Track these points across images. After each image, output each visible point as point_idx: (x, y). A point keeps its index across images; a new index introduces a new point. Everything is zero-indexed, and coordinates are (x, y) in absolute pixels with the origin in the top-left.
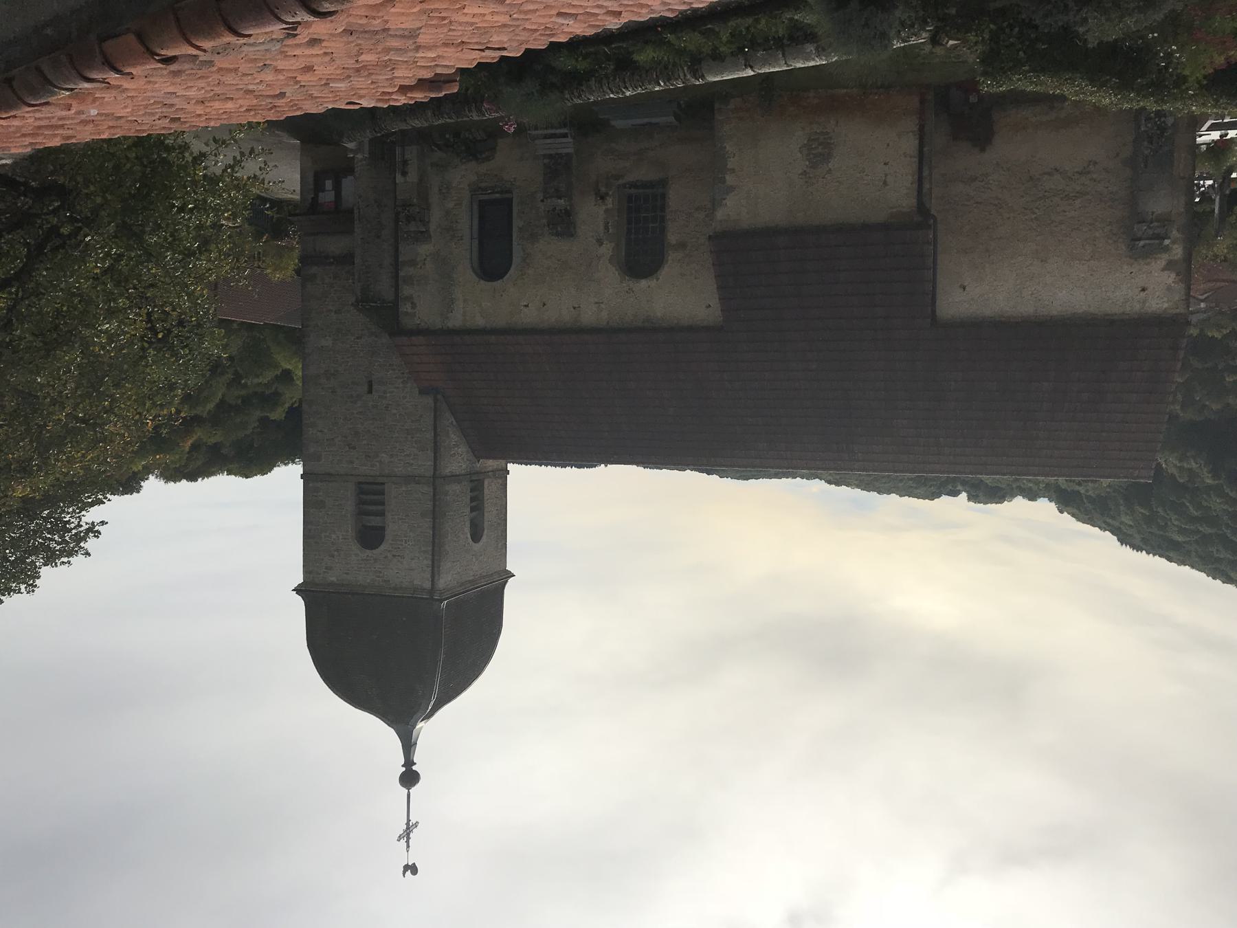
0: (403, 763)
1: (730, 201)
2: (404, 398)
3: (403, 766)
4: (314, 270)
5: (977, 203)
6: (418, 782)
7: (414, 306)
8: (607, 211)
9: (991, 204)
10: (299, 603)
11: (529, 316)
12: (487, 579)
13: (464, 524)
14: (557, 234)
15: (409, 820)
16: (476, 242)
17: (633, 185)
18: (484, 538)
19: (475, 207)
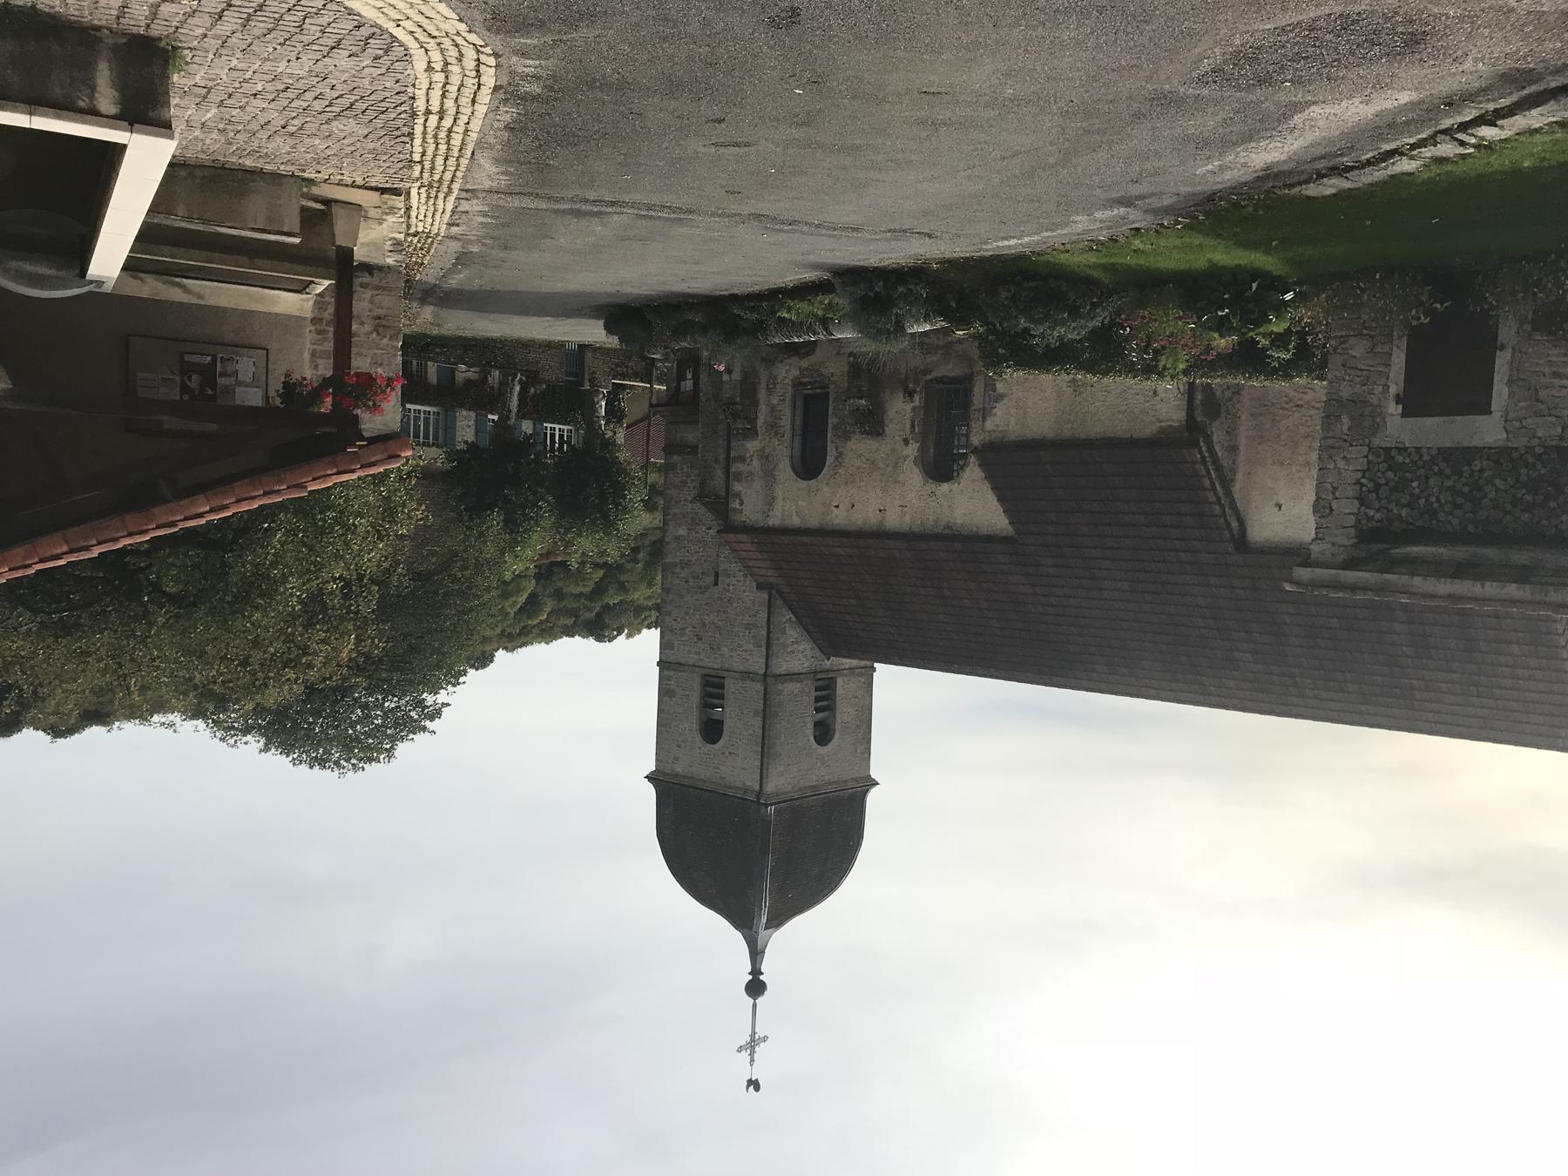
0: (750, 971)
1: (999, 410)
2: (744, 591)
3: (749, 974)
5: (1298, 406)
6: (763, 993)
7: (742, 503)
8: (914, 409)
9: (1313, 407)
10: (650, 792)
11: (839, 518)
12: (835, 786)
13: (805, 726)
14: (866, 432)
15: (754, 1033)
16: (798, 440)
17: (940, 380)
18: (835, 742)
19: (800, 404)
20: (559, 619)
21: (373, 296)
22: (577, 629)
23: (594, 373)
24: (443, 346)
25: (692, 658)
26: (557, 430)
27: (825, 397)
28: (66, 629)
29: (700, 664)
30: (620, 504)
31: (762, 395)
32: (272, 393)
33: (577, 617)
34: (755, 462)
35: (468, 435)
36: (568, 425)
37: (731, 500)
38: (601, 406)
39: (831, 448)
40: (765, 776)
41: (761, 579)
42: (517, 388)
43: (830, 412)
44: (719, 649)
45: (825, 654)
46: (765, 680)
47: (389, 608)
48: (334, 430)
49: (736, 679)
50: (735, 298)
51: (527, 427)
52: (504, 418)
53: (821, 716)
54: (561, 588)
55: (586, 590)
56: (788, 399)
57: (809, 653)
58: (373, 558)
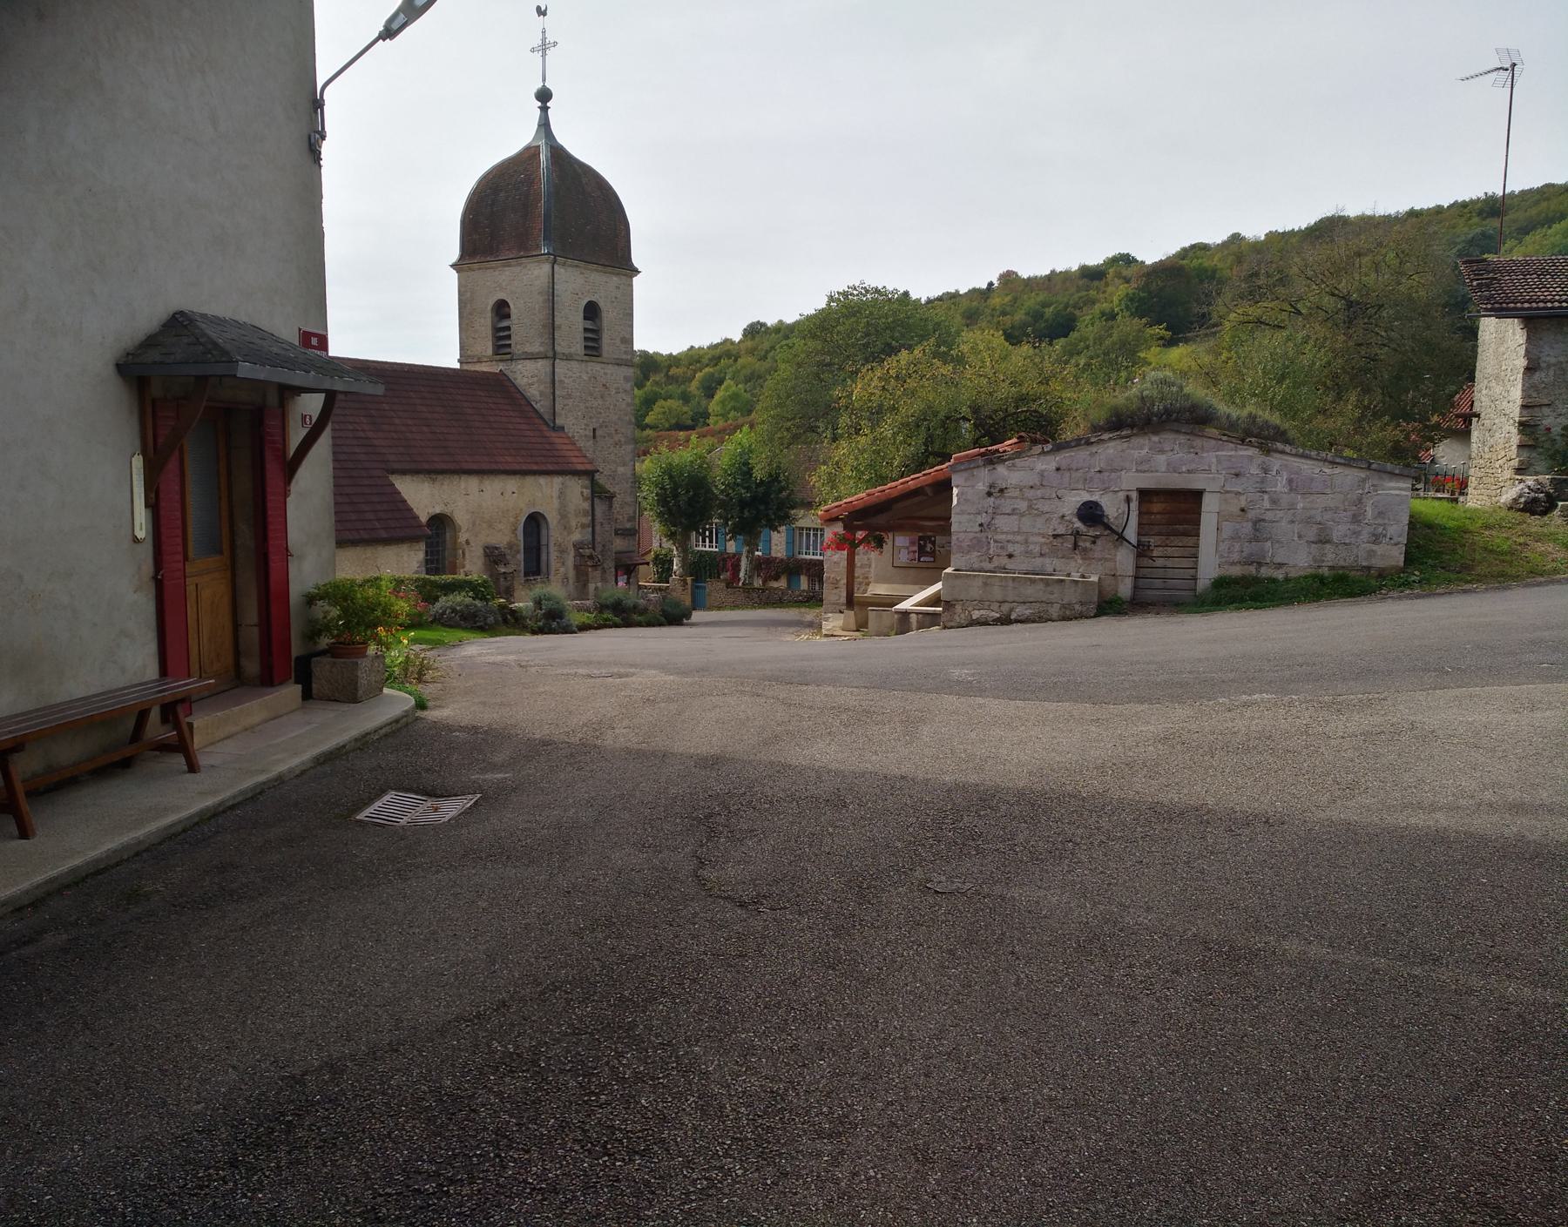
0: (549, 110)
2: (573, 425)
4: (628, 526)
7: (582, 493)
10: (637, 260)
11: (511, 484)
14: (496, 548)
15: (544, 56)
16: (544, 542)
18: (491, 302)
20: (684, 373)
21: (839, 599)
22: (666, 364)
23: (684, 590)
24: (796, 602)
25: (610, 369)
26: (707, 546)
27: (526, 574)
28: (1022, 399)
29: (603, 365)
30: (661, 489)
31: (571, 574)
32: (890, 543)
33: (667, 375)
34: (574, 524)
35: (776, 538)
36: (698, 551)
37: (590, 496)
38: (677, 565)
39: (521, 537)
40: (551, 277)
41: (561, 434)
42: (742, 574)
43: (523, 563)
44: (590, 378)
45: (505, 375)
46: (555, 353)
47: (829, 411)
48: (855, 523)
49: (576, 354)
50: (616, 626)
51: (732, 547)
52: (751, 552)
53: (505, 324)
54: (684, 404)
55: (661, 403)
56: (552, 573)
57: (519, 377)
58: (843, 448)
